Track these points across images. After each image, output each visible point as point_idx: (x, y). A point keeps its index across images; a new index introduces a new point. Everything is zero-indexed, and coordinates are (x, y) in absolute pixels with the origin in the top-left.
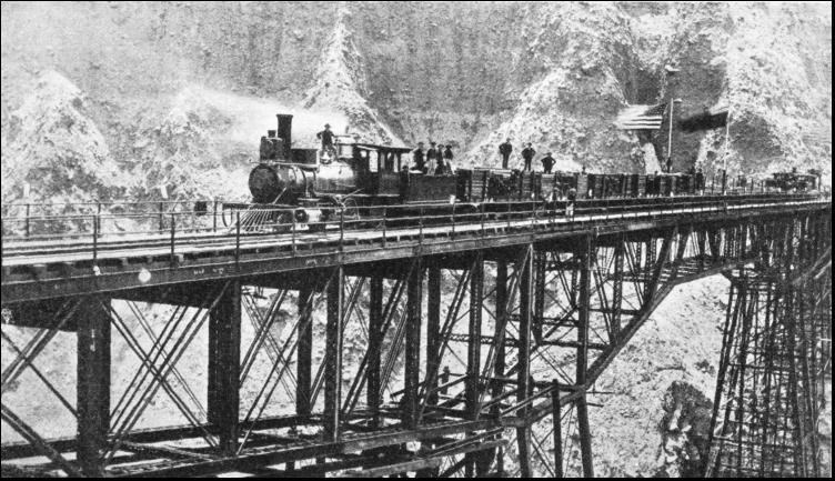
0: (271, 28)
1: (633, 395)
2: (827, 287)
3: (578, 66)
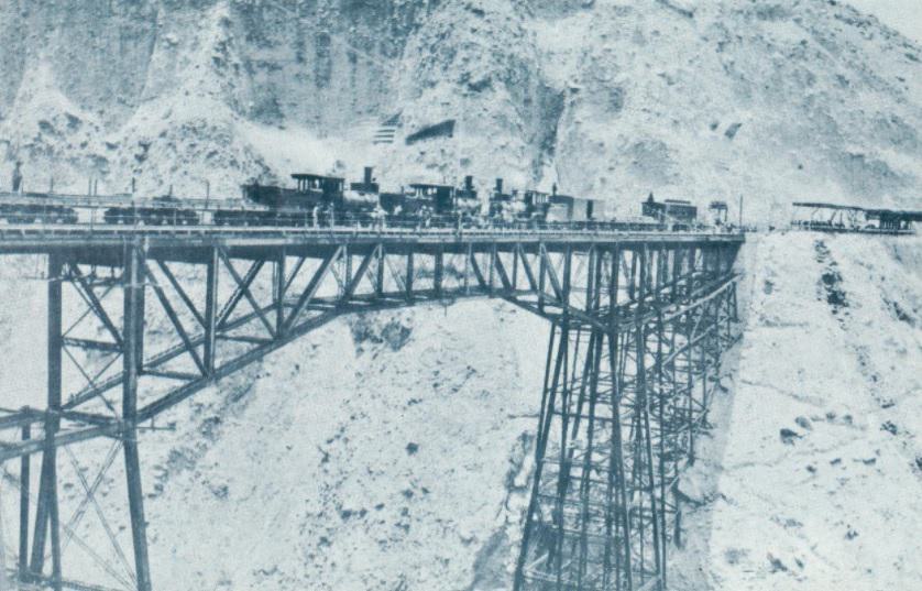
0: (144, 31)
1: (480, 445)
2: (216, 318)
3: (465, 79)
